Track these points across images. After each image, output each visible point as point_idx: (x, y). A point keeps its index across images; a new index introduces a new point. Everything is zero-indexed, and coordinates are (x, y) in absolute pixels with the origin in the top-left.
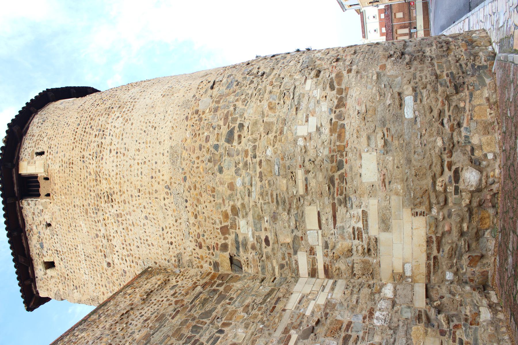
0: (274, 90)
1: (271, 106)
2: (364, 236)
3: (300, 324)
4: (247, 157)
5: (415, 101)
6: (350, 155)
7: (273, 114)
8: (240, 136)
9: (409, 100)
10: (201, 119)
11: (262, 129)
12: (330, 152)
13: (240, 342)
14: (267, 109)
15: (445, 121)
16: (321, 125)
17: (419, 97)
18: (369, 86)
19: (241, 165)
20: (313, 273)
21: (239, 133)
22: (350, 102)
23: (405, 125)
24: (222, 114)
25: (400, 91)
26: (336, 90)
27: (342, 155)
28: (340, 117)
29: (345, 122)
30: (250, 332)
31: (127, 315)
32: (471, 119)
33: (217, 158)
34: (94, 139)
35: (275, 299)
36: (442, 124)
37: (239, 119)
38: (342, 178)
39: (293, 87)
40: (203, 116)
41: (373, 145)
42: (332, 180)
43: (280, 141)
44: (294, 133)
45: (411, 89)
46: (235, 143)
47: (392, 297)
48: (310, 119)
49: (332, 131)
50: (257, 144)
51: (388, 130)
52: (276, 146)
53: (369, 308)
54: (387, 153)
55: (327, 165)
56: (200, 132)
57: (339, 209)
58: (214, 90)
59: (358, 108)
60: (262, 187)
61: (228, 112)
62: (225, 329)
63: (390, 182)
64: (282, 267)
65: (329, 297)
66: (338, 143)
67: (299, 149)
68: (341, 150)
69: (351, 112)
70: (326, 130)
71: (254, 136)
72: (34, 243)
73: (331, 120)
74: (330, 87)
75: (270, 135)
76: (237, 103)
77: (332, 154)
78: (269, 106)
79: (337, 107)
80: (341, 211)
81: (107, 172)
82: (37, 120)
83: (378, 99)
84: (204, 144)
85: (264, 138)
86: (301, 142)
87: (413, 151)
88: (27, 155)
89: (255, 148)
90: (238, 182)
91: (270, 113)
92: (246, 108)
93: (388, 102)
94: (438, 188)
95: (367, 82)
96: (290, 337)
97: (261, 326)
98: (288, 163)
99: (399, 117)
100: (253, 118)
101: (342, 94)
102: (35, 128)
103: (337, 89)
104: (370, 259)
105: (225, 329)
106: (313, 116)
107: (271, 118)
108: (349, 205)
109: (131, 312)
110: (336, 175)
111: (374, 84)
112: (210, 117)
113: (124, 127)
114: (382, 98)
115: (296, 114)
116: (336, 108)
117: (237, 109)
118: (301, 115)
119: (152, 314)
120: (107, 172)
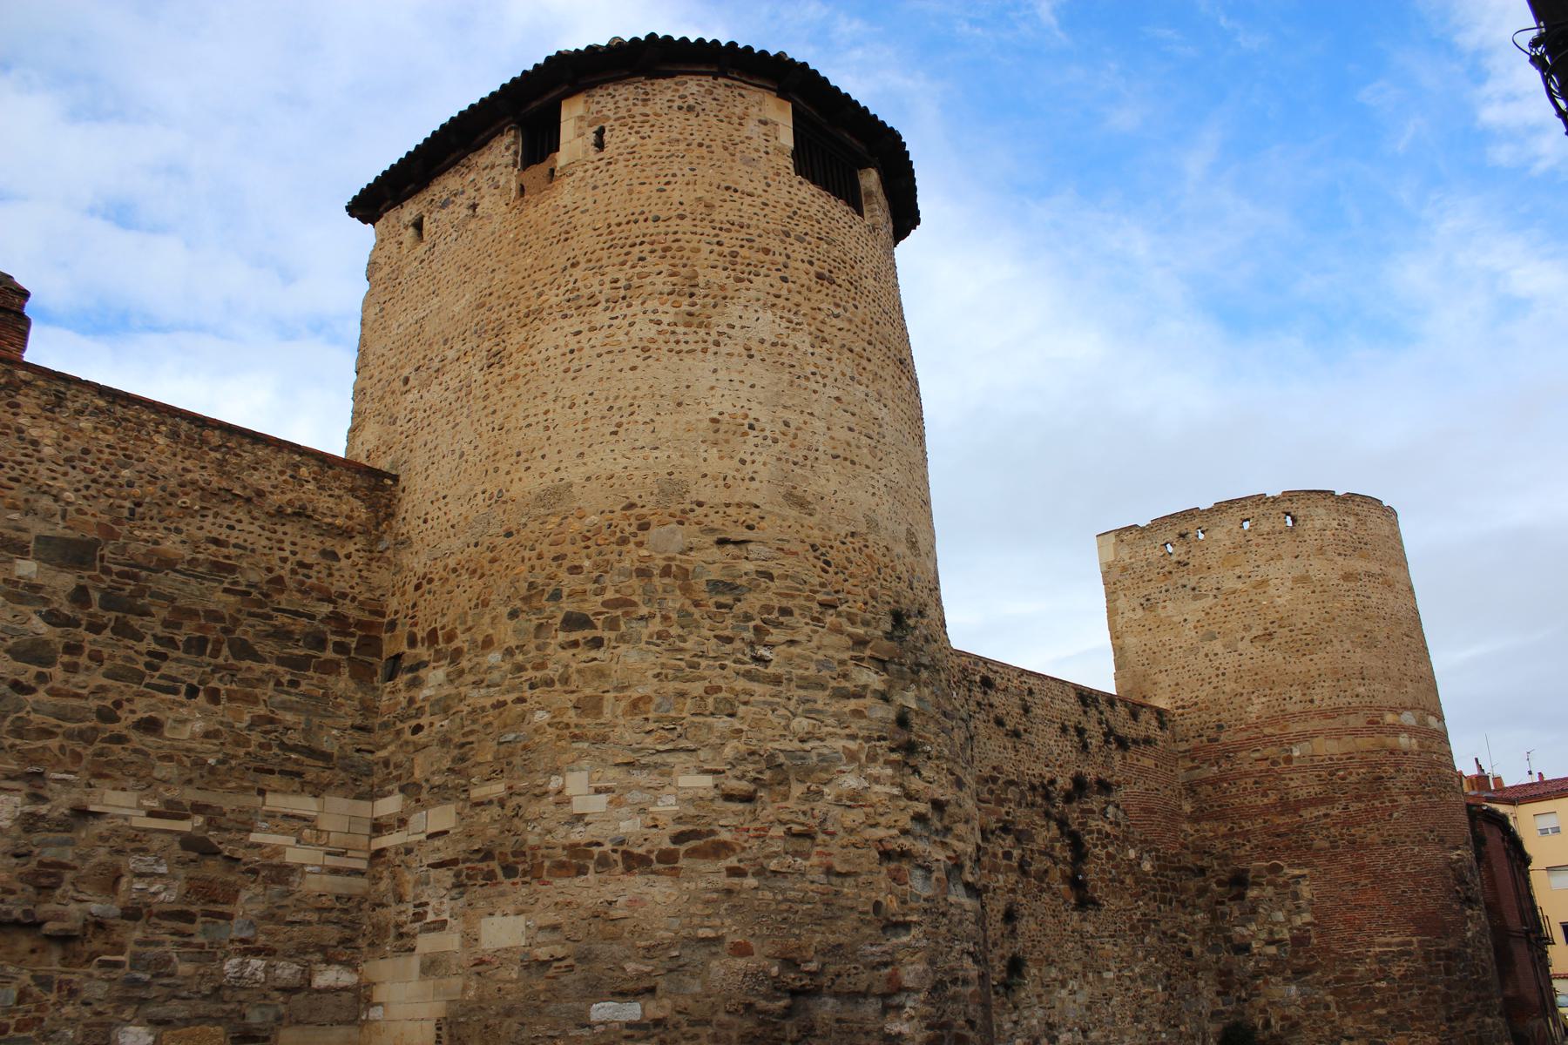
0: (689, 701)
1: (641, 705)
2: (417, 925)
3: (219, 828)
4: (533, 668)
5: (629, 1025)
6: (524, 891)
7: (619, 712)
8: (575, 644)
9: (632, 1011)
10: (624, 541)
11: (588, 691)
12: (532, 848)
13: (167, 734)
14: (635, 695)
16: (587, 824)
17: (638, 1033)
18: (676, 924)
19: (520, 658)
20: (378, 828)
21: (582, 641)
22: (636, 883)
23: (576, 1005)
24: (630, 591)
25: (659, 993)
27: (525, 873)
28: (604, 863)
29: (591, 876)
30: (195, 745)
33: (535, 603)
34: (607, 279)
35: (296, 768)
37: (613, 635)
38: (490, 876)
39: (692, 746)
40: (631, 546)
41: (541, 937)
42: (488, 855)
44: (574, 766)
45: (660, 1014)
46: (562, 636)
47: (315, 985)
48: (604, 798)
49: (573, 849)
50: (558, 686)
51: (570, 968)
52: (549, 730)
53: (277, 946)
54: (526, 967)
55: (510, 843)
56: (594, 549)
57: (451, 873)
58: (715, 549)
59: (621, 900)
60: (483, 709)
61: (634, 604)
62: (201, 699)
63: (479, 974)
64: (386, 763)
65: (308, 869)
66: (547, 864)
67: (540, 782)
68: (535, 872)
69: (611, 887)
70: (578, 835)
71: (575, 677)
72: (450, 182)
73: (599, 844)
74: (682, 833)
75: (572, 713)
76: (658, 619)
77: (528, 853)
78: (640, 699)
79: (627, 855)
80: (447, 876)
81: (538, 339)
82: (693, 87)
83: (638, 943)
84: (566, 563)
87: (524, 1020)
88: (598, 107)
89: (549, 683)
90: (494, 657)
91: (623, 704)
92: (643, 645)
93: (631, 967)
95: (692, 916)
98: (517, 760)
99: (595, 990)
100: (614, 667)
101: (659, 861)
102: (669, 94)
103: (677, 851)
104: (391, 939)
105: (201, 699)
106: (610, 802)
107: (611, 708)
108: (454, 893)
109: (238, 502)
110: (494, 865)
111: (684, 933)
112: (627, 564)
113: (629, 350)
114: (642, 952)
115: (617, 765)
116: (624, 852)
117: (643, 623)
118: (613, 776)
119: (235, 546)
120: (538, 339)
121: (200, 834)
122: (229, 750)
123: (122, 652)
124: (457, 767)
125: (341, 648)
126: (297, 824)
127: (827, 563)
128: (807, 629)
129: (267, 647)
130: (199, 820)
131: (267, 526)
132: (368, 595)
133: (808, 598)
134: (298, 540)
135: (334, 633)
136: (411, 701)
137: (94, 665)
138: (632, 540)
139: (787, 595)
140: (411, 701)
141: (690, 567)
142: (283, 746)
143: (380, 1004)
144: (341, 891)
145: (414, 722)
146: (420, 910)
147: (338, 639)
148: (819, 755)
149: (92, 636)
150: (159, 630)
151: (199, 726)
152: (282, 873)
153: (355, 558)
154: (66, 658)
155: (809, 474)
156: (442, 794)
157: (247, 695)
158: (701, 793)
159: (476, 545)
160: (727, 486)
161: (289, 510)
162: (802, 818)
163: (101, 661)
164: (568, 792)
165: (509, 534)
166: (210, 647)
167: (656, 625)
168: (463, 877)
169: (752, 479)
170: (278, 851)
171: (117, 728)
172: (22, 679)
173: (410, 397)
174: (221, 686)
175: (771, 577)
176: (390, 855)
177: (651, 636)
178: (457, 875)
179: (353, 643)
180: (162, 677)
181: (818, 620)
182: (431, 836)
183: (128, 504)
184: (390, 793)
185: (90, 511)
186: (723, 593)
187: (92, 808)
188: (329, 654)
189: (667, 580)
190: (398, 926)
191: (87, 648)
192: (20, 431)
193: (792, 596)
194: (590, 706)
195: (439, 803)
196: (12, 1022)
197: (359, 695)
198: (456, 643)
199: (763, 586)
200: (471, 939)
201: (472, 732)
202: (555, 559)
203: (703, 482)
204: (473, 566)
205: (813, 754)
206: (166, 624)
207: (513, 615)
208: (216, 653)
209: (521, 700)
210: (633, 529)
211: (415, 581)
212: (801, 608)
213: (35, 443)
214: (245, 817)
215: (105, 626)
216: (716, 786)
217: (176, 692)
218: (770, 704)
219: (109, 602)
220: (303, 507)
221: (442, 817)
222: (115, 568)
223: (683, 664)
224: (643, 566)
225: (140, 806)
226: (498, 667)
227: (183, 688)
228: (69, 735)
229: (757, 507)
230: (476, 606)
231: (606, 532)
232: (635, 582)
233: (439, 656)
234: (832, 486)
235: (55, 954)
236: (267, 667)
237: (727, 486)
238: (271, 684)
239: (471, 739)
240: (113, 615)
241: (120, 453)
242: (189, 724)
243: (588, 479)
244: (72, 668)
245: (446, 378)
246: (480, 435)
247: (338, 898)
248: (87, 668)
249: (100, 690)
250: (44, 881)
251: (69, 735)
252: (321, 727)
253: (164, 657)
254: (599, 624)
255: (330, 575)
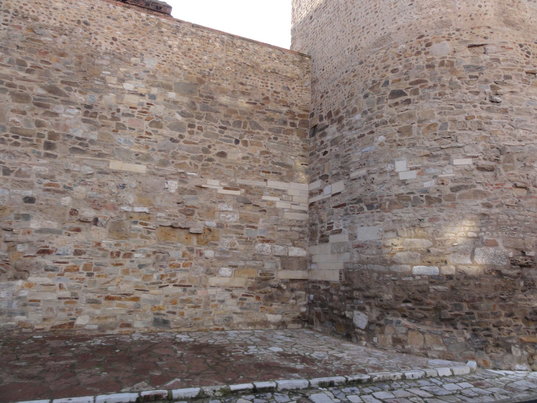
2: (329, 231)
4: (377, 118)
7: (421, 132)
8: (397, 104)
10: (419, 53)
15: (410, 305)
26: (452, 193)
27: (377, 208)
30: (240, 162)
31: (245, 66)
32: (409, 329)
33: (376, 89)
36: (406, 301)
37: (416, 97)
40: (423, 55)
42: (359, 201)
43: (391, 147)
46: (390, 102)
48: (415, 172)
50: (389, 124)
52: (386, 144)
55: (369, 194)
57: (343, 210)
60: (354, 139)
61: (426, 81)
70: (402, 190)
73: (413, 193)
75: (397, 135)
76: (439, 87)
78: (432, 125)
79: (428, 197)
80: (341, 211)
85: (394, 129)
86: (389, 168)
89: (385, 123)
90: (358, 117)
94: (355, 292)
96: (237, 189)
97: (246, 168)
105: (240, 145)
106: (418, 174)
108: (345, 217)
117: (431, 90)
121: (243, 196)
122: (252, 164)
123: (210, 127)
124: (343, 165)
125: (293, 125)
126: (280, 193)
127: (528, 53)
128: (520, 86)
129: (265, 125)
130: (243, 190)
131: (261, 77)
132: (302, 104)
133: (519, 70)
134: (273, 82)
135: (290, 119)
136: (322, 142)
137: (200, 131)
138: (423, 52)
139: (508, 69)
140: (322, 142)
141: (454, 60)
142: (273, 163)
143: (315, 263)
144: (298, 219)
145: (324, 151)
146: (330, 225)
147: (292, 121)
148: (530, 147)
149: (198, 121)
150: (223, 118)
151: (240, 155)
152: (276, 211)
153: (296, 89)
154: (189, 129)
155: (516, 10)
156: (337, 177)
157: (258, 143)
158: (467, 167)
159: (346, 72)
160: (472, 19)
161: (269, 71)
162: (522, 179)
163: (202, 130)
164: (397, 171)
165: (361, 63)
166: (242, 124)
167: (438, 90)
168: (349, 210)
169: (486, 14)
170: (273, 203)
171: (210, 156)
172: (173, 137)
173: (313, 23)
174: (248, 140)
175: (497, 60)
176: (317, 204)
177: (436, 95)
178: (346, 210)
179: (297, 123)
180: (225, 136)
181: (526, 81)
182: (333, 195)
183: (208, 70)
184: (315, 180)
185: (193, 73)
186: (473, 71)
187: (203, 186)
188: (288, 127)
189: (443, 68)
190: (321, 232)
191: (197, 125)
192: (165, 42)
193: (511, 70)
194: (408, 130)
195: (336, 181)
196: (181, 264)
197: (301, 143)
198: (340, 114)
199: (495, 65)
200: (353, 237)
201: (349, 150)
202: (384, 68)
203: (459, 19)
204: (345, 81)
205: (526, 147)
206: (225, 116)
207: (366, 96)
208: (245, 127)
209: (372, 132)
210: (424, 47)
211: (321, 95)
212: (517, 75)
213: (170, 46)
214: (260, 190)
215: (203, 117)
216: (474, 164)
217: (231, 142)
218: (501, 123)
219: (204, 108)
220: (274, 69)
221: (338, 186)
222: (205, 95)
223: (453, 107)
224: (430, 63)
225: (220, 185)
226: (360, 120)
227: (234, 140)
228: (193, 158)
229: (489, 27)
230: (348, 97)
231: (409, 51)
232: (426, 71)
233: (333, 122)
234: (528, 15)
235: (194, 239)
236: (265, 132)
237: (472, 19)
238: (267, 139)
239: (349, 152)
240: (205, 112)
241: (202, 49)
242: (236, 154)
243: (399, 29)
244: (192, 133)
245: (328, 8)
246: (345, 26)
247: (297, 221)
248: (197, 133)
249: (203, 141)
250: (188, 213)
251: (193, 158)
252: (287, 156)
253: (225, 128)
254: (408, 93)
255: (287, 96)
